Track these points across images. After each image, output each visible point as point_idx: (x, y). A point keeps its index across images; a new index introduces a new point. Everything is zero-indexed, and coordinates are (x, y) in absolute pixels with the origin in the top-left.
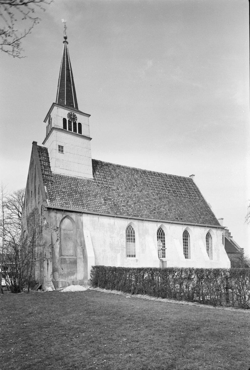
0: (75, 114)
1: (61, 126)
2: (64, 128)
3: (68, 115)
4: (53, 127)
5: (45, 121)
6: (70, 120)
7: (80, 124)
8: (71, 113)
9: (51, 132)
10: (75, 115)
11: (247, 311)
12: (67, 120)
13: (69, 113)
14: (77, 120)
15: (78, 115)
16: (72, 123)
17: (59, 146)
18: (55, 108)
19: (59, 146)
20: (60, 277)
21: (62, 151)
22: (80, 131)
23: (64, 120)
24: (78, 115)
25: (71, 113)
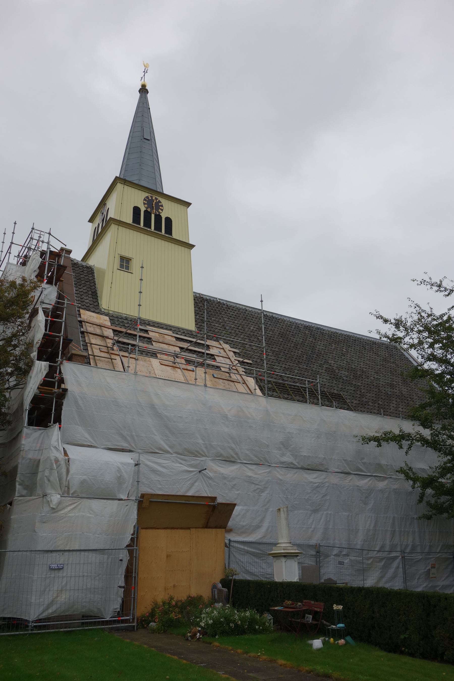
0: (159, 201)
1: (129, 219)
2: (134, 221)
3: (145, 200)
4: (113, 217)
5: (91, 220)
6: (149, 210)
7: (169, 221)
8: (152, 197)
9: (105, 229)
10: (160, 202)
11: (1, 616)
12: (143, 209)
13: (147, 197)
14: (162, 210)
15: (164, 202)
16: (153, 216)
17: (122, 259)
18: (119, 186)
19: (122, 259)
20: (26, 378)
21: (127, 268)
22: (169, 230)
23: (136, 210)
24: (164, 202)
25: (152, 197)
